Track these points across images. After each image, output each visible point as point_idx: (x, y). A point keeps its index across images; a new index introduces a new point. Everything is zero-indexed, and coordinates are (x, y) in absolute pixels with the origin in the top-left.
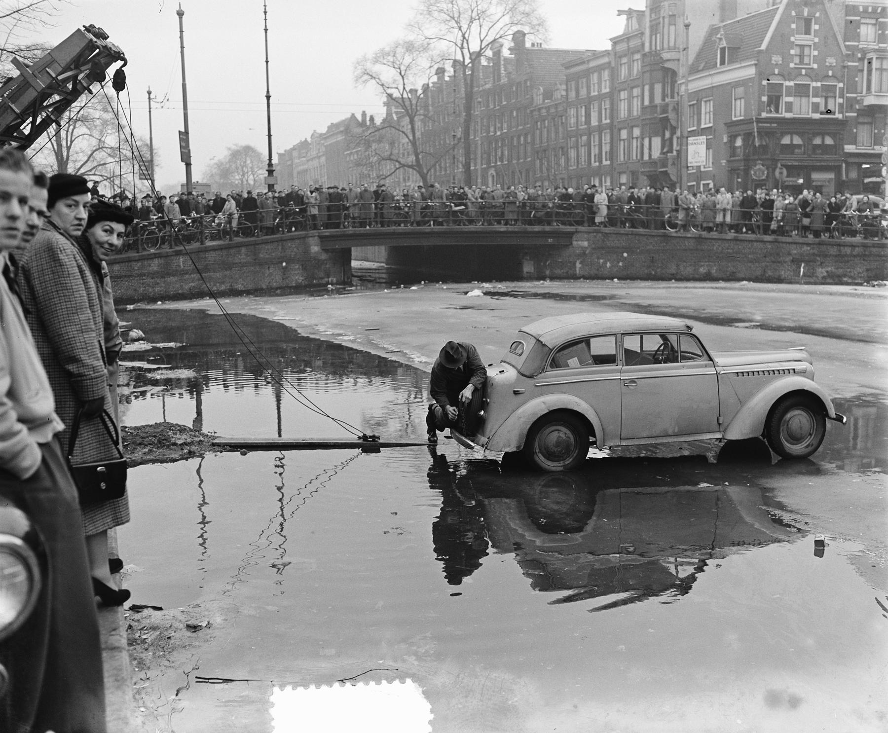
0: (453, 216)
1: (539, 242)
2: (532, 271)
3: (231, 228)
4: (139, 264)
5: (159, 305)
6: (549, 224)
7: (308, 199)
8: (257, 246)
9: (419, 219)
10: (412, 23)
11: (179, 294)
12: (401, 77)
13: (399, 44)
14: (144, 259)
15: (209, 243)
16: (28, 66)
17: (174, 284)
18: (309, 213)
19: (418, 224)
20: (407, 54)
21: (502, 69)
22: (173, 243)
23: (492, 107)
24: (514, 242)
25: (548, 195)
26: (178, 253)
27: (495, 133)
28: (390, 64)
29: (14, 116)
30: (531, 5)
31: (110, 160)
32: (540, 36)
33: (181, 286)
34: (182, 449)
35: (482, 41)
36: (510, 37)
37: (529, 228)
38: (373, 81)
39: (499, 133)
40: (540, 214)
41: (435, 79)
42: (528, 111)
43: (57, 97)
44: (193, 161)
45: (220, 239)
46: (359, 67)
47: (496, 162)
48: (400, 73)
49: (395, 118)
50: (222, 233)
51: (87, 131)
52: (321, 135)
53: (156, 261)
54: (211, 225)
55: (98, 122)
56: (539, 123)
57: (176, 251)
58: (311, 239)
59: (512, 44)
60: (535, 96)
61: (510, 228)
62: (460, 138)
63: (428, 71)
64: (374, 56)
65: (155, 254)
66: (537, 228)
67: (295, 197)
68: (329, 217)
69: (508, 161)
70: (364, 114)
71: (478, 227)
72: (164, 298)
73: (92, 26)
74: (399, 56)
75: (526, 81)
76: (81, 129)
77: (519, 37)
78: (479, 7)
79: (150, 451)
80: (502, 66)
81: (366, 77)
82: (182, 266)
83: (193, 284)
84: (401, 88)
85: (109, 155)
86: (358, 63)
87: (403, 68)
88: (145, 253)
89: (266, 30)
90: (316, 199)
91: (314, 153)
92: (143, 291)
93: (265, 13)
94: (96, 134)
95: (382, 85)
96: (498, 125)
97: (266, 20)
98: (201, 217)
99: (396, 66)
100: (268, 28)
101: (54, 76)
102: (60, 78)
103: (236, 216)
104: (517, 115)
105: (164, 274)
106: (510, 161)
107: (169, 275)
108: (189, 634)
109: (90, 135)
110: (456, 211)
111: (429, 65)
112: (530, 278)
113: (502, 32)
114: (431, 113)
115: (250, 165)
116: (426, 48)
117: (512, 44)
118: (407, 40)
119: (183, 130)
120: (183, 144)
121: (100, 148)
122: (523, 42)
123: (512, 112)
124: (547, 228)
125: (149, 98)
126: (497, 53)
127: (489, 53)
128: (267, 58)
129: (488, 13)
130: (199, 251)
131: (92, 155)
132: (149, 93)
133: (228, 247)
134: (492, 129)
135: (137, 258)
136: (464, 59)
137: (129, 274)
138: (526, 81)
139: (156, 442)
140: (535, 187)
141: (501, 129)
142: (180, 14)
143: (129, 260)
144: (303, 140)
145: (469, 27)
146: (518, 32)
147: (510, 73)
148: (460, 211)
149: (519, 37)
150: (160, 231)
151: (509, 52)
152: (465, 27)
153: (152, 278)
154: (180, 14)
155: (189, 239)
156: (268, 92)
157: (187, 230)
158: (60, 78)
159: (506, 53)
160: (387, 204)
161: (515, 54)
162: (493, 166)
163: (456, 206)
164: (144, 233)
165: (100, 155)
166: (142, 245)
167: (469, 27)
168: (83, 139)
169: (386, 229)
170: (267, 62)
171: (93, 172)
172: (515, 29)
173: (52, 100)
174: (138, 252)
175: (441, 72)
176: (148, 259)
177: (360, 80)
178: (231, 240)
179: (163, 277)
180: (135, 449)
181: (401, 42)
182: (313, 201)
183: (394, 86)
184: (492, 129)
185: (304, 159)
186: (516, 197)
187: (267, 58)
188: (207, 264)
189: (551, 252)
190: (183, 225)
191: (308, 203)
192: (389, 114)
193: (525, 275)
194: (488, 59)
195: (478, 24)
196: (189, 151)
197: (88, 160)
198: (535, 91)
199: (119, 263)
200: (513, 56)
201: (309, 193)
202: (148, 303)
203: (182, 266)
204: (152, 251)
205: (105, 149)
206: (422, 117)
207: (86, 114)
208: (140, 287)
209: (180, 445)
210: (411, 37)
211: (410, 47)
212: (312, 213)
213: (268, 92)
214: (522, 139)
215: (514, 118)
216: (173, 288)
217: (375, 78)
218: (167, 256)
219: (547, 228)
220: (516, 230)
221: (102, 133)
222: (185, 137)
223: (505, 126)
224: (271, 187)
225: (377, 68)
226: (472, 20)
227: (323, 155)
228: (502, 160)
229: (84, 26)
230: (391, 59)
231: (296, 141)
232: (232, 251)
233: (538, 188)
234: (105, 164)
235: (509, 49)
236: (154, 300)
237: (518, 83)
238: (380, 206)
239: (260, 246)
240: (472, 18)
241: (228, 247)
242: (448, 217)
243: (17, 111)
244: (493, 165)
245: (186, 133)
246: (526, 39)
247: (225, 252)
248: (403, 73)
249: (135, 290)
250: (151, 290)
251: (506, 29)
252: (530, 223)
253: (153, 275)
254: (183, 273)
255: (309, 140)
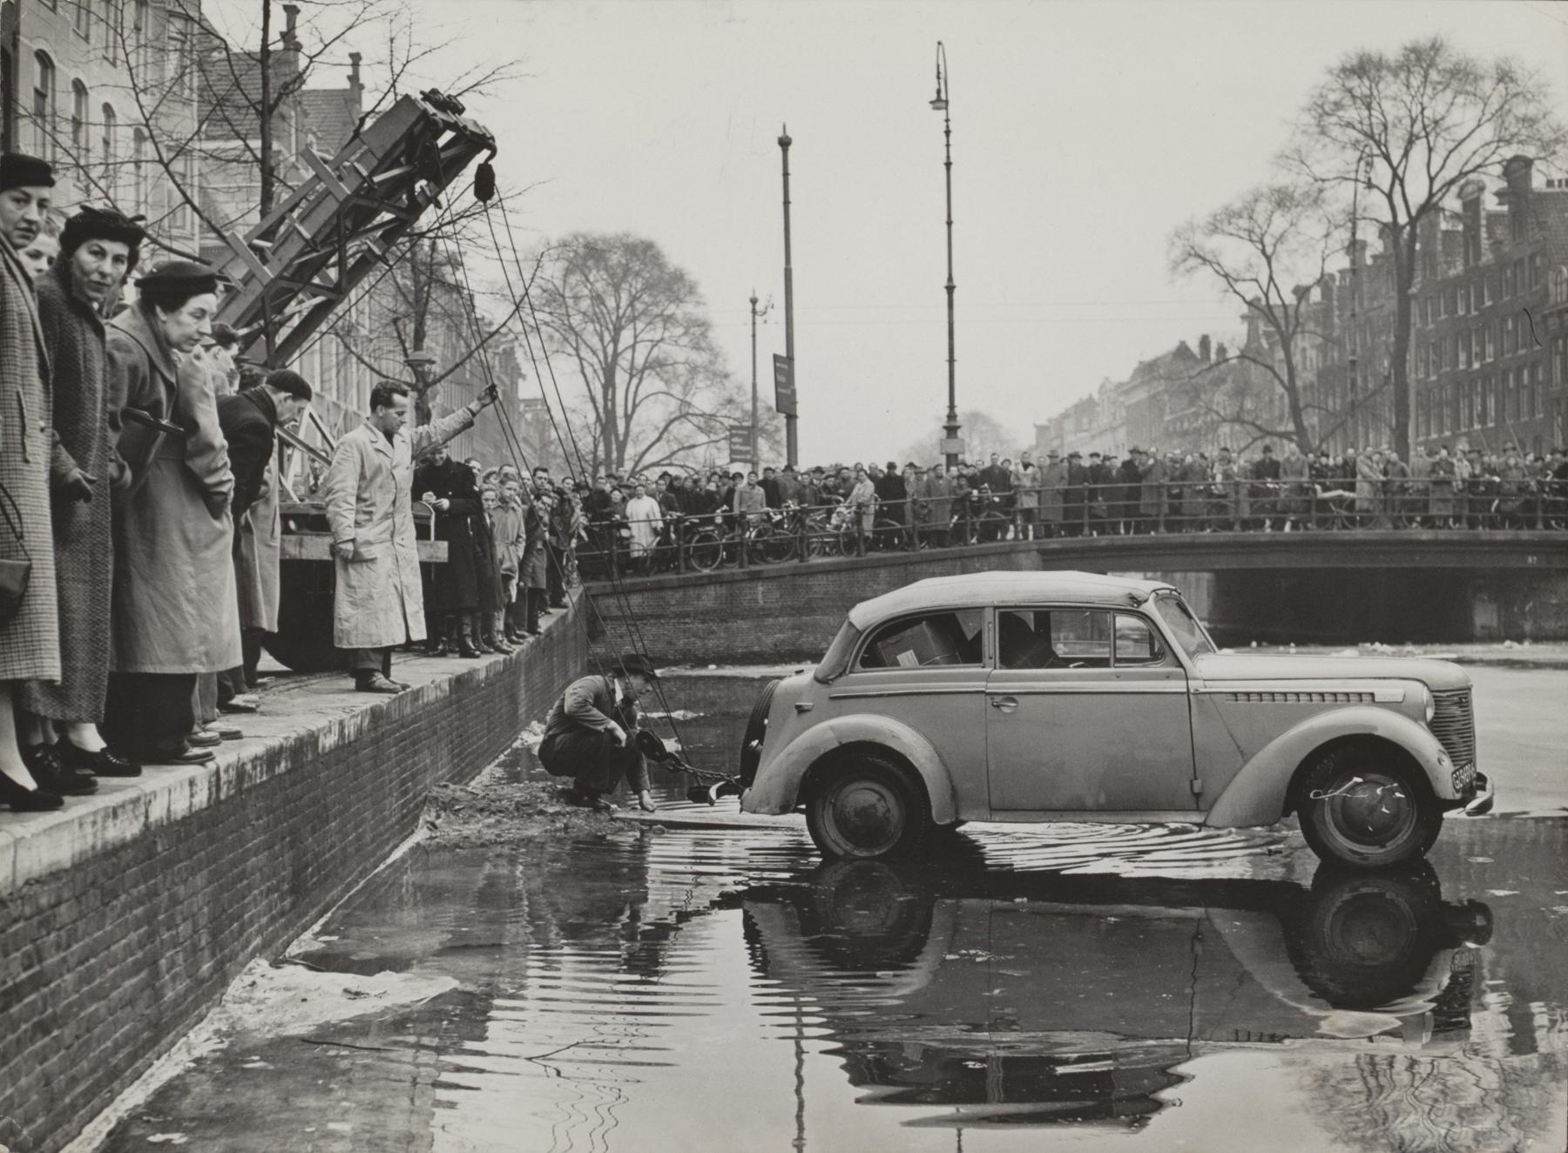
0: (1318, 511)
1: (1514, 562)
2: (1494, 623)
3: (861, 531)
4: (679, 595)
5: (712, 670)
6: (1531, 525)
7: (1018, 479)
8: (911, 568)
9: (1246, 513)
10: (1287, 152)
11: (752, 653)
12: (1264, 260)
13: (1262, 195)
14: (689, 586)
15: (815, 560)
16: (326, 162)
17: (745, 634)
18: (1018, 506)
19: (1246, 525)
20: (1277, 214)
21: (1484, 234)
22: (746, 558)
23: (1461, 313)
24: (1452, 562)
25: (1527, 467)
26: (756, 577)
27: (1469, 364)
28: (1245, 234)
29: (302, 243)
30: (1539, 102)
31: (702, 438)
32: (1558, 163)
33: (759, 639)
34: (553, 821)
35: (1432, 180)
36: (1498, 170)
37: (1483, 533)
38: (1208, 269)
39: (1476, 365)
40: (1511, 506)
41: (1339, 262)
42: (1538, 318)
43: (386, 216)
44: (800, 410)
45: (839, 553)
46: (1179, 243)
47: (1471, 425)
48: (1263, 252)
49: (1266, 346)
50: (850, 542)
51: (661, 386)
52: (1120, 385)
53: (712, 591)
54: (823, 529)
55: (681, 369)
56: (1560, 342)
57: (750, 573)
58: (1022, 556)
59: (1503, 184)
60: (1551, 286)
61: (1443, 535)
62: (1388, 377)
63: (1322, 244)
64: (1211, 220)
65: (709, 577)
66: (1501, 535)
67: (996, 476)
68: (1067, 513)
69: (1496, 421)
70: (1205, 342)
71: (1383, 531)
72: (721, 660)
73: (434, 91)
74: (1261, 218)
75: (1532, 258)
76: (651, 383)
77: (1517, 169)
78: (1427, 113)
79: (499, 822)
80: (1483, 230)
81: (1193, 262)
82: (761, 602)
83: (782, 636)
84: (1264, 280)
85: (699, 428)
86: (1178, 235)
87: (1268, 240)
88: (691, 575)
89: (948, 165)
90: (1034, 479)
91: (1104, 420)
92: (685, 644)
93: (948, 133)
94: (677, 390)
95: (1226, 276)
96: (1475, 349)
97: (948, 145)
98: (803, 511)
99: (1255, 238)
100: (952, 160)
101: (365, 173)
102: (377, 179)
103: (872, 509)
104: (1515, 326)
105: (726, 614)
106: (1499, 419)
107: (735, 616)
108: (344, 1000)
109: (667, 394)
110: (1325, 502)
111: (1324, 232)
112: (1491, 637)
113: (1477, 160)
114: (1336, 333)
115: (979, 449)
116: (1316, 200)
117: (1503, 184)
118: (1276, 186)
119: (783, 353)
120: (782, 379)
121: (683, 416)
122: (1527, 177)
123: (1504, 321)
124: (1525, 534)
125: (754, 312)
126: (1472, 205)
127: (1452, 203)
128: (949, 216)
129: (1445, 124)
130: (796, 574)
131: (666, 428)
132: (754, 301)
133: (851, 568)
134: (1462, 357)
135: (676, 583)
136: (1395, 216)
137: (659, 611)
138: (1532, 258)
139: (511, 808)
140: (1505, 451)
141: (1482, 356)
142: (785, 143)
143: (660, 587)
144: (1085, 397)
145: (1406, 154)
146: (1516, 158)
147: (1501, 243)
148: (1333, 500)
149: (1517, 169)
150: (722, 534)
151: (1496, 200)
152: (1396, 157)
153: (703, 622)
154: (785, 143)
155: (779, 550)
156: (950, 279)
157: (774, 534)
158: (377, 179)
159: (1490, 203)
160: (1190, 486)
161: (1509, 203)
162: (1465, 434)
163: (1326, 489)
164: (692, 538)
165: (683, 429)
166: (687, 560)
167: (1406, 154)
168: (655, 402)
169: (1187, 536)
170: (949, 223)
171: (667, 461)
172: (1508, 152)
173: (378, 220)
174: (678, 573)
175: (1355, 247)
176: (695, 586)
177: (1181, 268)
178: (859, 555)
179: (723, 621)
180: (471, 816)
181: (1265, 190)
182: (1027, 483)
183: (1248, 276)
184: (1462, 357)
185: (1084, 434)
186: (1452, 472)
187: (949, 216)
188: (810, 600)
189: (1535, 585)
190: (768, 526)
191: (1018, 487)
192: (1252, 334)
193: (1478, 631)
194: (1455, 216)
195: (1426, 146)
196: (794, 392)
197: (658, 440)
198: (1551, 275)
199: (641, 591)
200: (1505, 208)
201: (1021, 467)
202: (693, 667)
203: (761, 602)
204: (706, 571)
205: (690, 417)
206: (1320, 340)
207: (662, 356)
208: (678, 638)
209: (552, 814)
210: (1284, 179)
211: (1283, 200)
212: (1026, 506)
213: (950, 279)
214: (1526, 373)
215: (1508, 332)
216: (743, 641)
217: (1210, 262)
218: (732, 581)
219: (1525, 534)
220: (1456, 537)
221: (686, 388)
222: (786, 367)
223: (1490, 349)
224: (952, 459)
225: (1212, 244)
226: (1411, 141)
227: (1123, 424)
228: (1483, 420)
229: (422, 93)
230: (1244, 223)
231: (1071, 401)
232: (861, 575)
233: (1511, 453)
234: (693, 446)
235: (1498, 194)
236: (703, 662)
237: (1515, 264)
238: (1176, 491)
239: (918, 568)
240: (1411, 134)
241: (851, 568)
242: (1308, 511)
243: (307, 235)
244: (1464, 430)
245: (790, 359)
246: (1534, 171)
247: (845, 577)
248: (1269, 250)
249: (670, 643)
250: (699, 643)
251: (1488, 151)
252: (1493, 524)
253: (705, 616)
254: (765, 613)
255: (1096, 396)
